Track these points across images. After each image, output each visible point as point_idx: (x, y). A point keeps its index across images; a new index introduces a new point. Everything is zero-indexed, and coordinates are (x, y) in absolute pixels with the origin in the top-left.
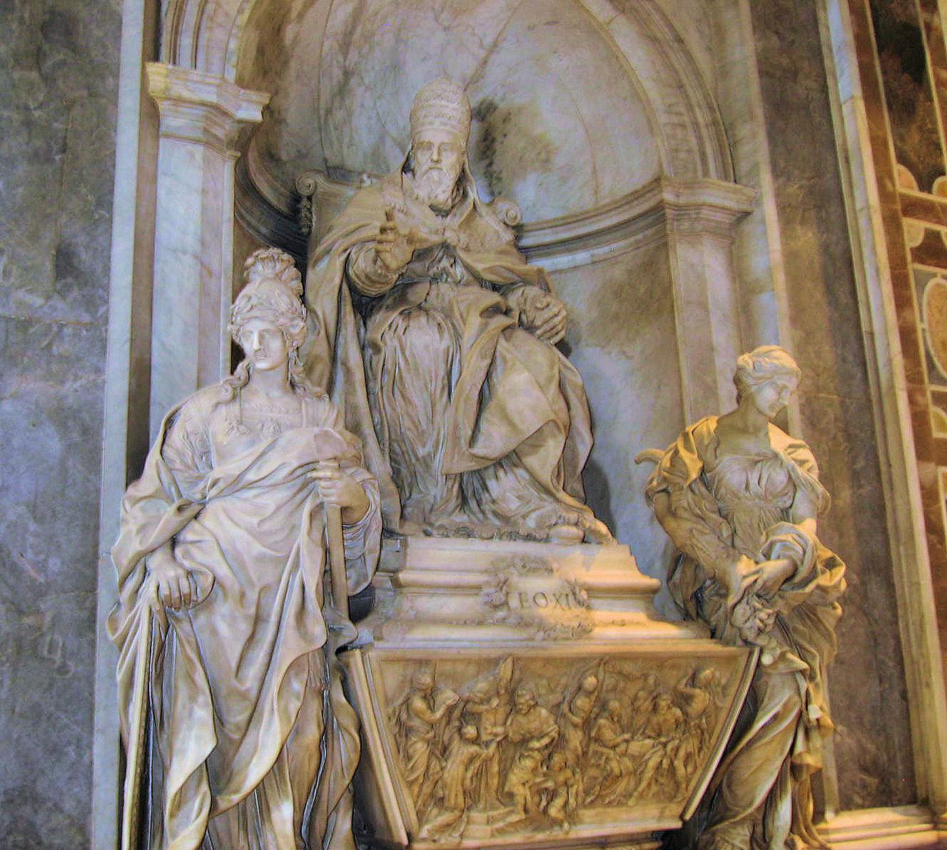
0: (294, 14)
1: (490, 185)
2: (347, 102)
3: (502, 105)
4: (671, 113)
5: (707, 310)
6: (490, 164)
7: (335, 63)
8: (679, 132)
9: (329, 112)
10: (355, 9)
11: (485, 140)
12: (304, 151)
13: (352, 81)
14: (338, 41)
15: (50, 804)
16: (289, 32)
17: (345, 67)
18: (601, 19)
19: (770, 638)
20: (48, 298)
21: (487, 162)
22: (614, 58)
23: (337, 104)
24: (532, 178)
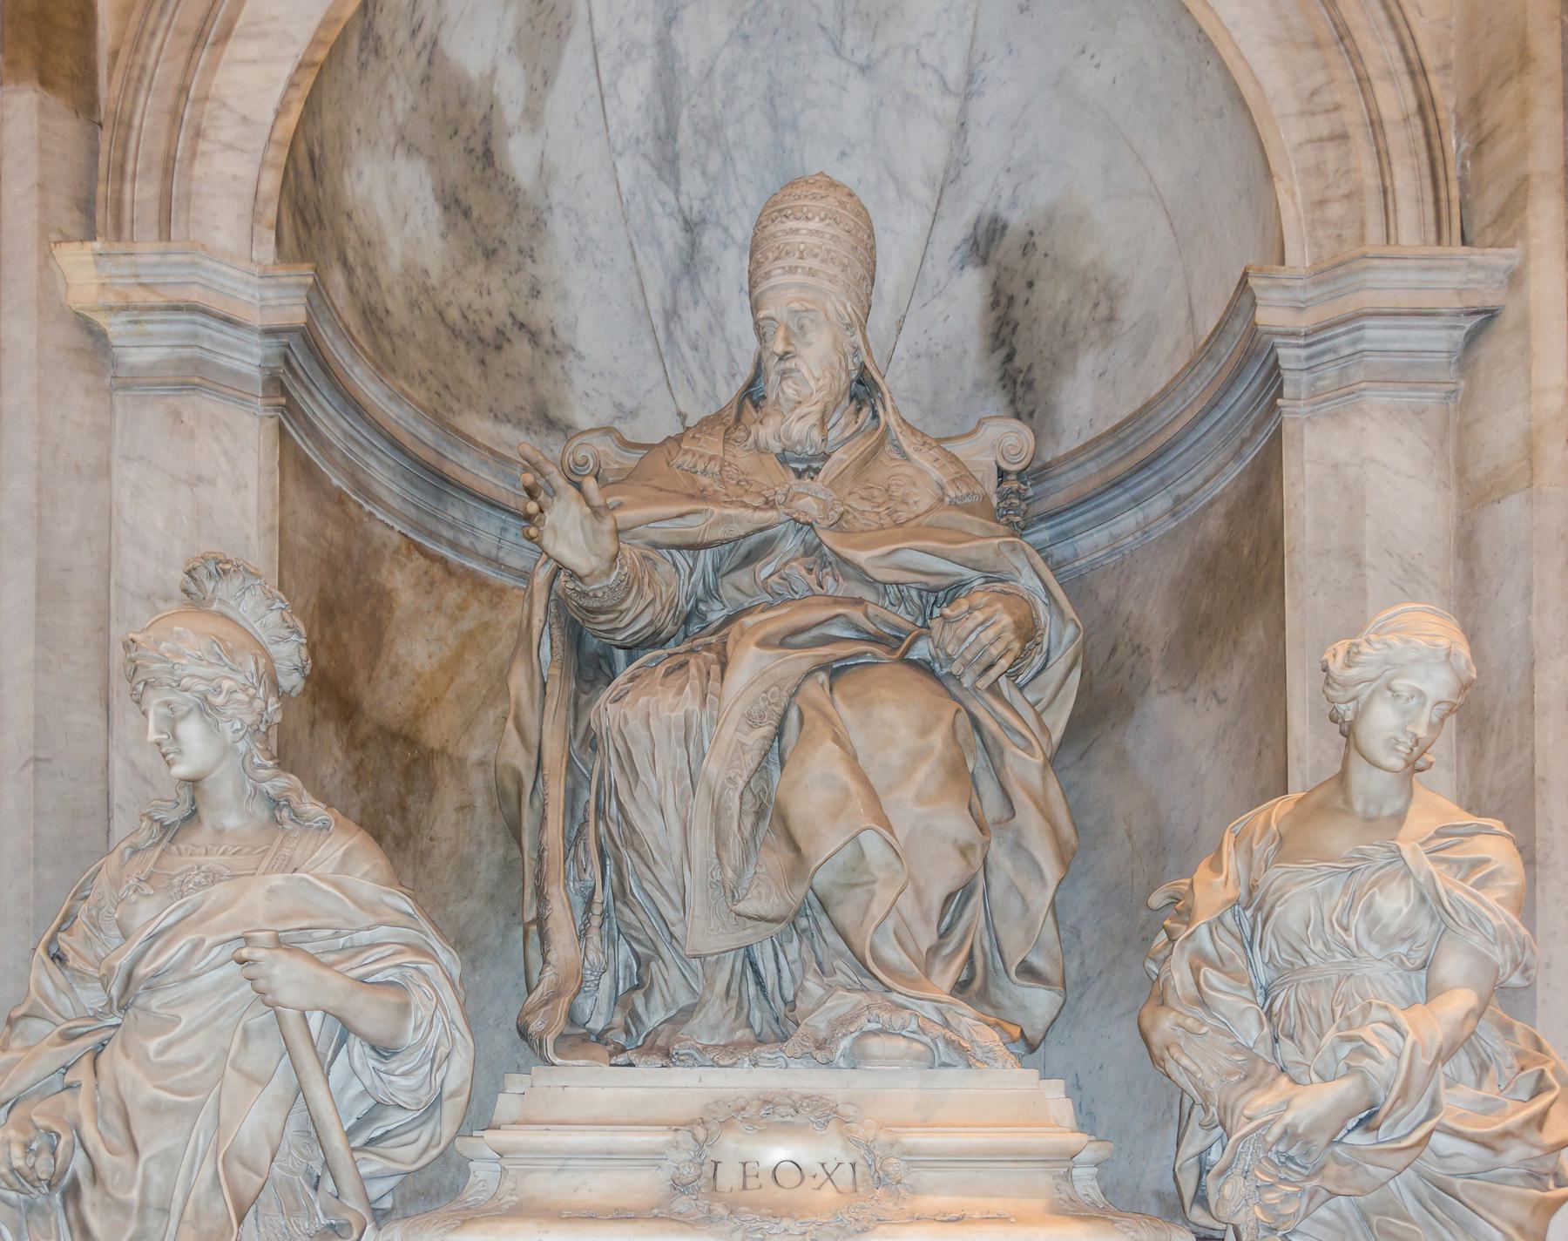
0: (512, 113)
1: (1012, 402)
2: (708, 287)
3: (1016, 220)
4: (1313, 114)
5: (1359, 564)
6: (1010, 358)
7: (657, 208)
8: (1331, 153)
9: (671, 315)
10: (658, 74)
11: (995, 305)
12: (630, 404)
14: (645, 156)
16: (519, 156)
17: (681, 210)
23: (684, 296)
24: (1087, 363)
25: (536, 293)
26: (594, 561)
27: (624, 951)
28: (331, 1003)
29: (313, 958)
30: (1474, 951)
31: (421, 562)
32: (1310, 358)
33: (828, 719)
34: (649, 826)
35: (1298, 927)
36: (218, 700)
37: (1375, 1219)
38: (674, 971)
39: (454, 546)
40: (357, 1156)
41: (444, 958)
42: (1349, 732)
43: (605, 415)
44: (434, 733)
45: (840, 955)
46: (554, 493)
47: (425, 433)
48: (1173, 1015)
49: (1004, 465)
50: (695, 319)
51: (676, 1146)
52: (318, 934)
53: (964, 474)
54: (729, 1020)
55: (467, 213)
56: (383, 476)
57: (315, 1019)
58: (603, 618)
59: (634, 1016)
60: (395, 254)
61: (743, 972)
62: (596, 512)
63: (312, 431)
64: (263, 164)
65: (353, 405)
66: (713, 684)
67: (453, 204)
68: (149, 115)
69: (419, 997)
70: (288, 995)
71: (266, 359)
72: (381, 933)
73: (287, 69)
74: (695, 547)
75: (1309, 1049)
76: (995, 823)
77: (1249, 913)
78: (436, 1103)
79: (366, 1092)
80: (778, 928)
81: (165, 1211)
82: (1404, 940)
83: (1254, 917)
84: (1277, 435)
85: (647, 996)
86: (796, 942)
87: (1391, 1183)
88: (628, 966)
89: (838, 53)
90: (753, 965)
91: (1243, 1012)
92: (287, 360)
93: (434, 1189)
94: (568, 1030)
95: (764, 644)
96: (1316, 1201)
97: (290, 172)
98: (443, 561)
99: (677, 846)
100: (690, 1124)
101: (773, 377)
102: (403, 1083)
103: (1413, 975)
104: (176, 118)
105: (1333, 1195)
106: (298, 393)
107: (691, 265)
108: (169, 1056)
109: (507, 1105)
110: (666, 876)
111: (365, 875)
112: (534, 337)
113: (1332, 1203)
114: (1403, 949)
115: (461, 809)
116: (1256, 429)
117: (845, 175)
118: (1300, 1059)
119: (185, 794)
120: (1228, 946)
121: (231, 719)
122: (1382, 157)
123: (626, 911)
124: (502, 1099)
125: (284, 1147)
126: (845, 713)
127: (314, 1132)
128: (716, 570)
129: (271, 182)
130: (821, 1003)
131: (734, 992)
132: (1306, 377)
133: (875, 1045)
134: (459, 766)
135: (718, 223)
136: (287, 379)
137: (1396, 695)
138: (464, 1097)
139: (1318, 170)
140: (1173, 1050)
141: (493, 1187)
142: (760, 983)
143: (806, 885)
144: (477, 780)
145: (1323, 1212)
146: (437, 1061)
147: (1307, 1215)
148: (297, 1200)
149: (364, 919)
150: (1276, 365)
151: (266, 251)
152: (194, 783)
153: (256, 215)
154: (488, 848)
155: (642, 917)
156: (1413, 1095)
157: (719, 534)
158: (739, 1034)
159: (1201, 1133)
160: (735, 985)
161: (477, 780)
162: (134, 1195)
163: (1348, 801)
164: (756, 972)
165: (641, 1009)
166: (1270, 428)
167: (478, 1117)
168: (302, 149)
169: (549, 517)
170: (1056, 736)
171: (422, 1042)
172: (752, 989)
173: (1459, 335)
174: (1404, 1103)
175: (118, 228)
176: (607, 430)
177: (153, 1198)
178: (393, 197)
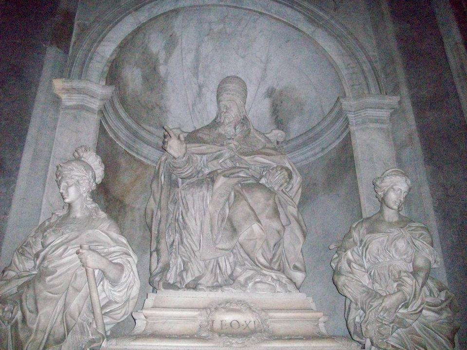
0: (161, 61)
2: (203, 100)
8: (354, 76)
9: (194, 105)
11: (273, 106)
13: (203, 89)
16: (162, 70)
19: (199, 284)
21: (276, 116)
22: (319, 49)
25: (162, 98)
27: (180, 260)
28: (102, 267)
30: (424, 257)
33: (242, 195)
34: (192, 224)
35: (376, 251)
36: (81, 182)
38: (195, 266)
39: (137, 154)
40: (104, 316)
41: (134, 257)
43: (177, 126)
44: (127, 201)
45: (247, 260)
48: (344, 277)
49: (278, 140)
53: (269, 141)
54: (212, 280)
56: (123, 133)
57: (97, 272)
58: (179, 170)
59: (183, 279)
61: (216, 265)
63: (107, 122)
64: (105, 65)
66: (210, 186)
67: (146, 79)
68: (80, 54)
69: (127, 267)
71: (99, 106)
72: (118, 248)
77: (361, 248)
78: (128, 300)
80: (227, 252)
82: (405, 254)
83: (363, 249)
85: (187, 272)
86: (232, 257)
90: (219, 264)
91: (364, 275)
92: (105, 108)
93: (124, 330)
95: (224, 176)
97: (111, 68)
100: (205, 308)
101: (223, 117)
103: (408, 264)
104: (86, 56)
107: (200, 94)
108: (51, 283)
109: (149, 302)
111: (114, 232)
112: (161, 108)
114: (405, 257)
119: (66, 208)
120: (357, 257)
122: (366, 78)
123: (182, 248)
126: (246, 195)
128: (207, 161)
129: (106, 69)
132: (354, 121)
133: (259, 286)
134: (132, 209)
135: (207, 87)
138: (136, 299)
139: (351, 79)
140: (346, 286)
143: (236, 240)
146: (130, 288)
149: (112, 243)
152: (70, 205)
154: (138, 232)
155: (187, 249)
160: (214, 269)
162: (35, 326)
163: (383, 217)
165: (184, 277)
166: (347, 131)
167: (140, 305)
171: (126, 282)
172: (218, 271)
174: (415, 300)
175: (69, 75)
177: (41, 328)
178: (133, 76)
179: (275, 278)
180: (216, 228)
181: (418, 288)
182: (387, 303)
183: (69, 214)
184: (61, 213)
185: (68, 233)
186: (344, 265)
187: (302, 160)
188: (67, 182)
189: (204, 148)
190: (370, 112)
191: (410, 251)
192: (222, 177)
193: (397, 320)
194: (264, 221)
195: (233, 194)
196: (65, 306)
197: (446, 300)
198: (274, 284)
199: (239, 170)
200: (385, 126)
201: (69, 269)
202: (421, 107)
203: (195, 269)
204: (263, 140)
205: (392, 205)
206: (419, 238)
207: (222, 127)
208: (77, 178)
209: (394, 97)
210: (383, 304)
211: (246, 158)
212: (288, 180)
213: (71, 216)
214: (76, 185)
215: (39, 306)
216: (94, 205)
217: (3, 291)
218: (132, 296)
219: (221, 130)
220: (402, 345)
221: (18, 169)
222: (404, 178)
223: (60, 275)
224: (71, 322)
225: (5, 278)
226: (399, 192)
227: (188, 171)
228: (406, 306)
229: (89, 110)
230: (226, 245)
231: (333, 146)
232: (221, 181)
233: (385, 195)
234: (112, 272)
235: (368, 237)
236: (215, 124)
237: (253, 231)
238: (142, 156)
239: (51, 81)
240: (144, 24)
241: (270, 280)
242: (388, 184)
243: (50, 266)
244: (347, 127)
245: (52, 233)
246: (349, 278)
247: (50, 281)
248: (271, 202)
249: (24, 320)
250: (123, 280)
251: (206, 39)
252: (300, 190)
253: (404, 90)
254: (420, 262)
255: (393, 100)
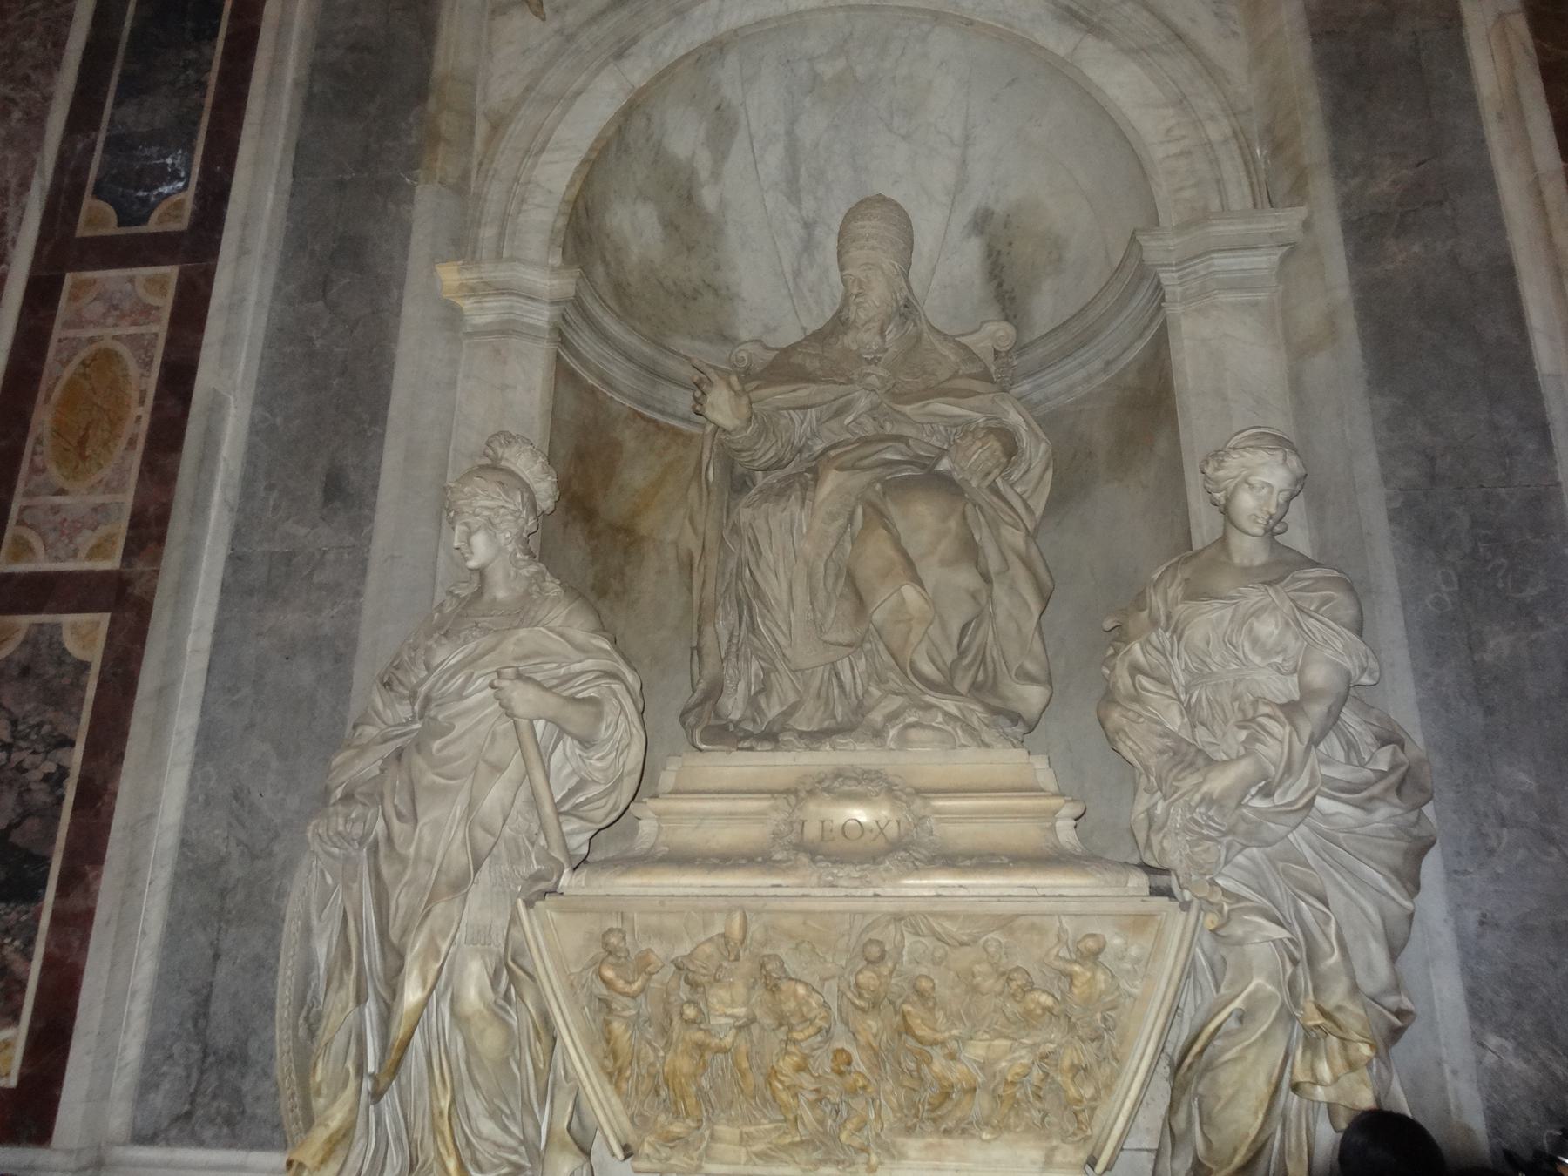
0: (704, 175)
3: (999, 209)
6: (1000, 285)
9: (797, 274)
11: (989, 256)
15: (258, 1069)
16: (708, 197)
18: (1061, 52)
20: (314, 526)
25: (718, 268)
26: (737, 422)
27: (755, 665)
29: (539, 684)
31: (643, 424)
32: (1180, 278)
34: (775, 588)
35: (1202, 645)
36: (497, 521)
37: (1280, 865)
39: (662, 412)
42: (1225, 511)
44: (644, 525)
45: (892, 669)
46: (711, 383)
47: (646, 349)
50: (811, 275)
51: (776, 809)
52: (547, 667)
53: (969, 355)
54: (819, 714)
55: (677, 228)
56: (620, 373)
57: (540, 725)
60: (635, 252)
62: (737, 394)
63: (576, 354)
64: (559, 213)
65: (604, 336)
67: (670, 225)
68: (494, 193)
69: (610, 709)
70: (521, 709)
72: (589, 664)
73: (575, 164)
74: (804, 408)
75: (1218, 732)
76: (998, 574)
79: (574, 772)
81: (430, 861)
84: (1164, 327)
85: (768, 698)
87: (1290, 836)
88: (757, 676)
89: (891, 131)
91: (1168, 707)
92: (563, 317)
94: (713, 722)
95: (840, 469)
96: (1233, 851)
98: (655, 421)
99: (785, 597)
100: (787, 792)
101: (853, 308)
102: (597, 763)
105: (1245, 847)
106: (569, 334)
107: (809, 245)
109: (668, 780)
110: (780, 617)
112: (716, 292)
113: (1247, 851)
114: (1278, 659)
115: (659, 572)
116: (1151, 320)
117: (895, 195)
118: (1212, 740)
119: (476, 577)
121: (504, 531)
124: (663, 775)
125: (514, 813)
127: (534, 802)
129: (562, 222)
130: (879, 701)
131: (823, 694)
132: (1179, 289)
133: (914, 734)
136: (563, 327)
137: (1252, 487)
141: (653, 840)
142: (841, 686)
144: (670, 553)
145: (1240, 859)
147: (1226, 862)
148: (519, 852)
149: (574, 654)
150: (1159, 283)
151: (556, 260)
152: (481, 572)
153: (552, 240)
156: (1296, 766)
157: (818, 399)
158: (826, 724)
159: (1147, 796)
161: (670, 553)
162: (412, 850)
163: (1229, 556)
164: (839, 679)
165: (764, 706)
166: (1159, 320)
168: (581, 203)
169: (710, 399)
170: (1038, 513)
172: (836, 691)
173: (1275, 258)
176: (757, 341)
177: (424, 852)
178: (635, 225)
179: (955, 711)
180: (821, 595)
181: (1299, 748)
182: (1219, 782)
183: (479, 593)
184: (464, 591)
185: (475, 637)
186: (1123, 680)
187: (1059, 394)
188: (466, 524)
189: (804, 393)
190: (1222, 262)
191: (1293, 644)
192: (834, 472)
193: (1242, 827)
194: (931, 572)
195: (860, 511)
196: (471, 806)
197: (1393, 768)
198: (949, 728)
199: (881, 446)
200: (1262, 296)
201: (480, 721)
202: (1366, 231)
203: (785, 689)
204: (952, 357)
205: (1246, 525)
206: (1316, 611)
207: (851, 334)
208: (486, 513)
209: (1289, 212)
210: (1205, 788)
211: (907, 409)
212: (1004, 460)
213: (486, 597)
214: (486, 528)
215: (420, 810)
216: (533, 568)
217: (353, 772)
218: (627, 768)
219: (849, 340)
220: (1256, 886)
221: (375, 487)
222: (1279, 455)
223: (463, 734)
224: (483, 840)
225: (357, 743)
226: (1265, 491)
227: (767, 452)
228: (1267, 793)
229: (529, 332)
230: (845, 636)
231: (1131, 355)
232: (832, 481)
233: (1228, 500)
234: (577, 718)
235: (1181, 609)
236: (840, 323)
237: (903, 601)
238: (674, 416)
239: (433, 270)
240: (643, 91)
241: (940, 719)
242: (1235, 473)
243: (440, 717)
244: (1159, 308)
245: (444, 641)
246: (1130, 714)
247: (439, 750)
248: (953, 524)
249: (389, 838)
250: (603, 734)
251: (807, 101)
252: (1049, 475)
253: (1323, 189)
254: (1318, 675)
255: (1288, 221)
